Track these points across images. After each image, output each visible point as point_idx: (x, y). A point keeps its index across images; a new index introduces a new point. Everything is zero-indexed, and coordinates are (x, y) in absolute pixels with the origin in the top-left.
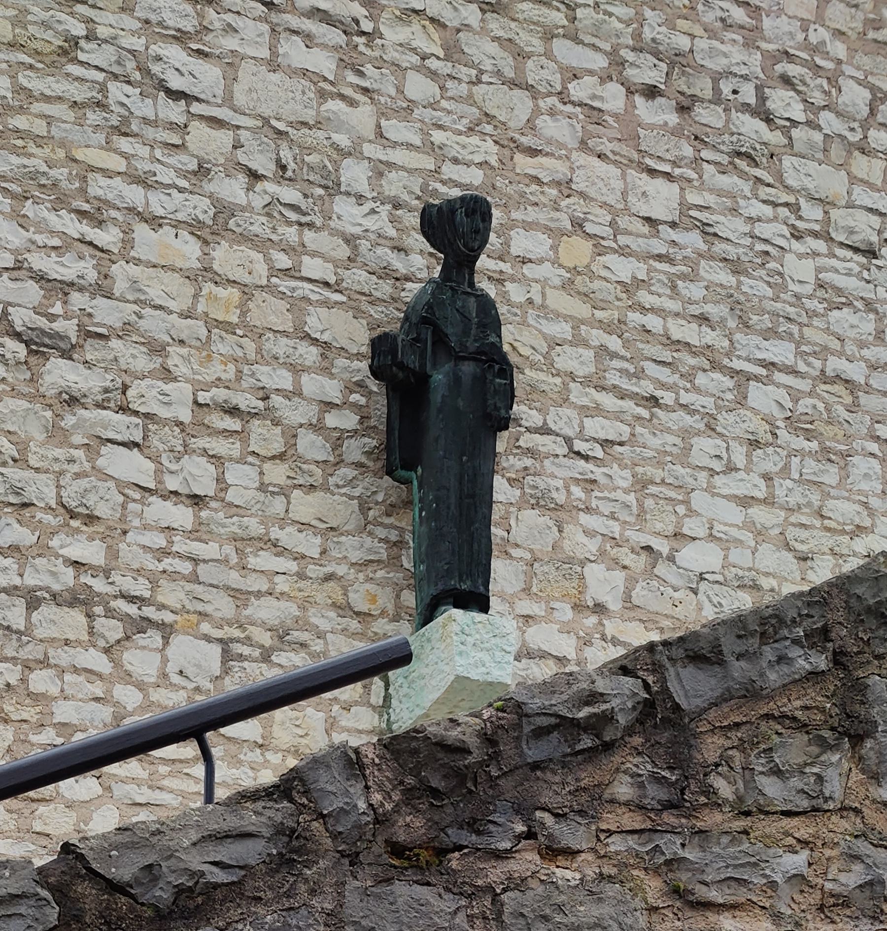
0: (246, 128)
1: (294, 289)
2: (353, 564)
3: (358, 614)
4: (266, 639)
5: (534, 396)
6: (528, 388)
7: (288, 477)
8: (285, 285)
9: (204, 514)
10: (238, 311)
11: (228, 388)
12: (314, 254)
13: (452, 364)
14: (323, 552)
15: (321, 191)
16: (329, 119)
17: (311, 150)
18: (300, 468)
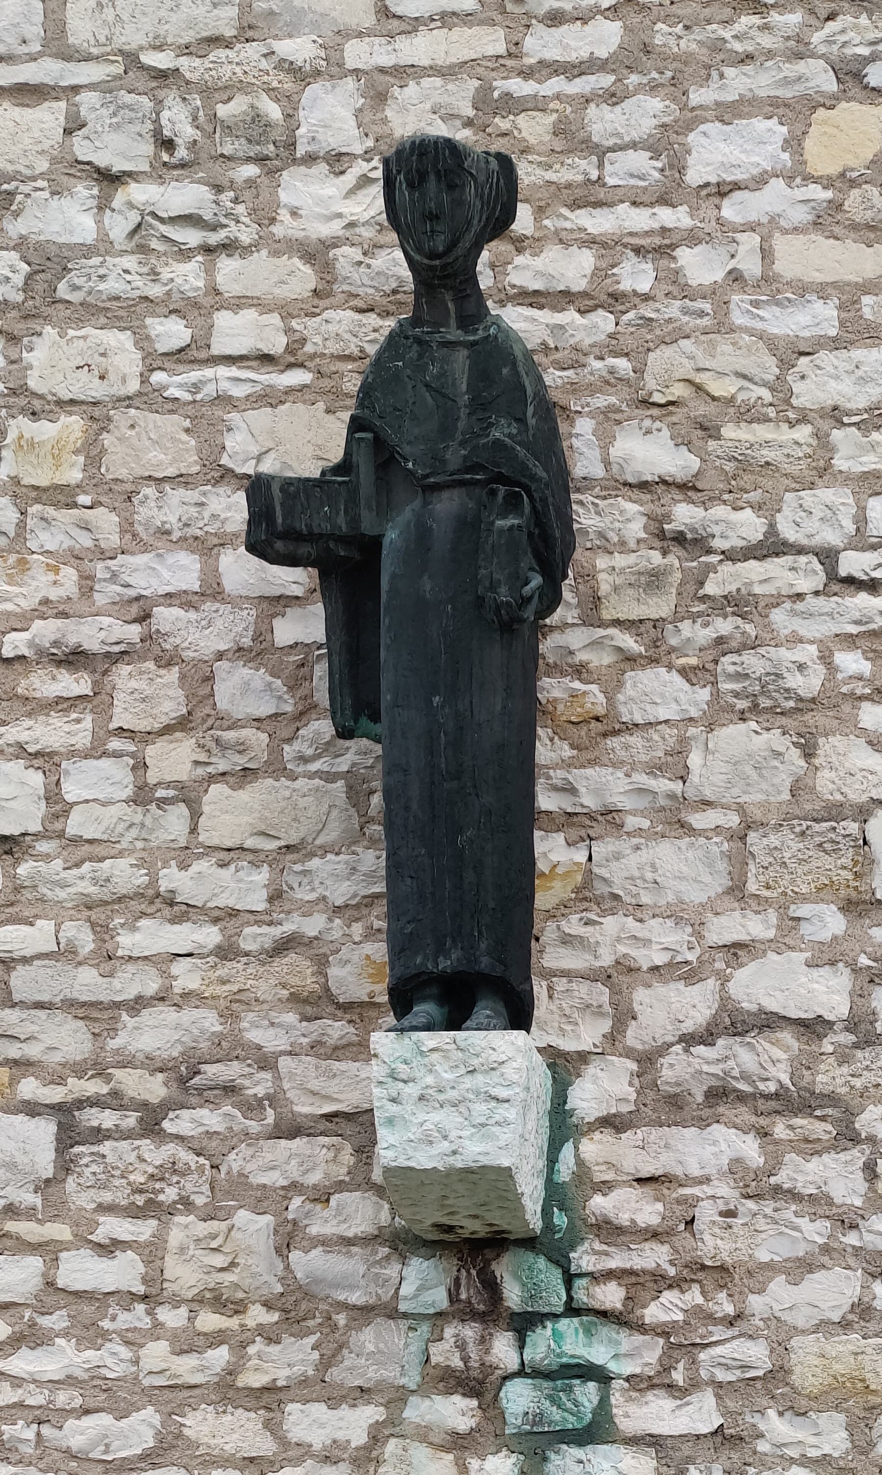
0: (91, 87)
1: (196, 387)
2: (338, 910)
3: (347, 1007)
4: (155, 1089)
5: (747, 479)
6: (729, 467)
7: (197, 763)
8: (174, 383)
9: (23, 870)
10: (81, 459)
11: (64, 615)
12: (238, 304)
13: (417, 503)
14: (276, 896)
15: (251, 170)
16: (272, 13)
17: (229, 90)
18: (217, 741)
